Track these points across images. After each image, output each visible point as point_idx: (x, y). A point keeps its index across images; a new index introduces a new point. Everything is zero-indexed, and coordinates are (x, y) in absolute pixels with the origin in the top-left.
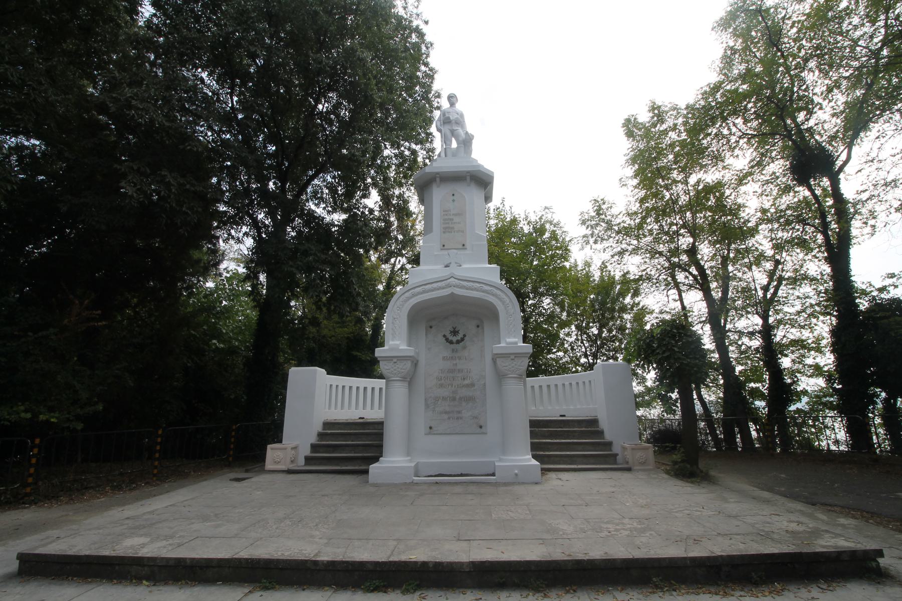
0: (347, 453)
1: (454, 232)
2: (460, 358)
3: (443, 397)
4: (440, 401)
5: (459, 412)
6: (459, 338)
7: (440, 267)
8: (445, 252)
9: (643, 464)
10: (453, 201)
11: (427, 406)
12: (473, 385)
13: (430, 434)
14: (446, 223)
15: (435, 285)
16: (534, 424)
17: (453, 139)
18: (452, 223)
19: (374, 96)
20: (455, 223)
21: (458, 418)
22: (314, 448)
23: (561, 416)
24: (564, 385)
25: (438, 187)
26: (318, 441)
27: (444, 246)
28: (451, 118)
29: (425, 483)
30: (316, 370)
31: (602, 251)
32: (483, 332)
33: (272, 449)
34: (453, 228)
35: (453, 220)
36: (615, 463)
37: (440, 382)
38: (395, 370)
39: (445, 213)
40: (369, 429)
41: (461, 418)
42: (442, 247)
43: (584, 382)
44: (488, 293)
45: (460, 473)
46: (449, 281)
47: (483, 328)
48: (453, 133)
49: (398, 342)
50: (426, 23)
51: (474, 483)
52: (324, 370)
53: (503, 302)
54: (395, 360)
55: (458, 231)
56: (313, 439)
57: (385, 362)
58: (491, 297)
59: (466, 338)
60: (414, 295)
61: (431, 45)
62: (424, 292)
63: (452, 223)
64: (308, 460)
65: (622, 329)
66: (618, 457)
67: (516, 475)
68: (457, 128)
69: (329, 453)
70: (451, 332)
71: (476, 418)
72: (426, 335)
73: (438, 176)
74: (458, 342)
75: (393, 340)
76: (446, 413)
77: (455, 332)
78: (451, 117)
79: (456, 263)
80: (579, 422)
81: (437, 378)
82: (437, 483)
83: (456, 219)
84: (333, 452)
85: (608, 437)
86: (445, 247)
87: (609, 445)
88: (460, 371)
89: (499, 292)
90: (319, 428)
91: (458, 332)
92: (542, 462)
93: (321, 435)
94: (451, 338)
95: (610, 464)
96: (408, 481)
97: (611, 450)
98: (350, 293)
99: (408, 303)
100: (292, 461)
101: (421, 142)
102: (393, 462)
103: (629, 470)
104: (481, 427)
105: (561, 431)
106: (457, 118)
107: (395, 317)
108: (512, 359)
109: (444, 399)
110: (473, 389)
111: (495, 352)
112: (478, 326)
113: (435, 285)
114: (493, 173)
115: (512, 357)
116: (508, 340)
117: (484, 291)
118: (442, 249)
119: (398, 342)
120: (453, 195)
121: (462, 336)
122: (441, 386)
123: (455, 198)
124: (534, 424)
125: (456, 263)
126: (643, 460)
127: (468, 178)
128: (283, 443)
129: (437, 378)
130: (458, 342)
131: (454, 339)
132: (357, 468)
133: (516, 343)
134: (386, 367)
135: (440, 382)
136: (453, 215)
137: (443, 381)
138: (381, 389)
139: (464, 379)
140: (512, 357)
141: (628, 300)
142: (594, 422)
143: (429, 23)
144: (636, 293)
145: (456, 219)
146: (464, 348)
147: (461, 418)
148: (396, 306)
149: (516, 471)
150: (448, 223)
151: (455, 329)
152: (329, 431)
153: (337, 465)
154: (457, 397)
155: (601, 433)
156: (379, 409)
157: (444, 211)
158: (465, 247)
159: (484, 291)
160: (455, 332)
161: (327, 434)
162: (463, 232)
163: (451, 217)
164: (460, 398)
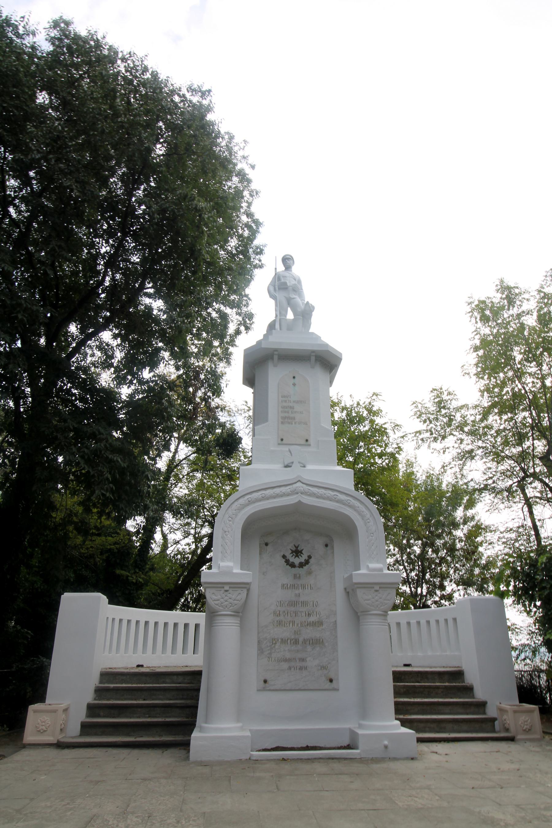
0: (139, 717)
1: (295, 423)
2: (303, 587)
3: (282, 639)
4: (278, 644)
5: (303, 660)
6: (302, 559)
7: (278, 466)
8: (286, 448)
9: (528, 731)
10: (294, 385)
11: (261, 651)
12: (320, 623)
13: (264, 689)
14: (285, 412)
15: (277, 491)
16: (398, 676)
17: (289, 309)
18: (292, 413)
19: (203, 252)
20: (296, 412)
21: (301, 668)
22: (92, 709)
23: (406, 665)
24: (409, 623)
25: (275, 366)
26: (95, 699)
27: (282, 440)
28: (288, 284)
29: (269, 760)
30: (100, 597)
31: (442, 451)
32: (333, 553)
33: (35, 711)
34: (294, 418)
35: (293, 408)
36: (494, 731)
37: (278, 618)
38: (226, 601)
39: (284, 399)
40: (164, 683)
41: (306, 668)
42: (280, 442)
43: (437, 621)
44: (344, 504)
45: (305, 746)
46: (295, 486)
47: (333, 548)
48: (290, 302)
49: (231, 564)
50: (253, 167)
51: (333, 759)
52: (105, 597)
53: (363, 517)
54: (227, 588)
55: (300, 423)
56: (89, 697)
57: (213, 590)
58: (348, 509)
59: (312, 561)
60: (250, 502)
61: (257, 193)
62: (264, 498)
63: (292, 413)
64: (86, 728)
65: (452, 549)
66: (496, 723)
67: (386, 747)
68: (294, 296)
69: (114, 717)
70: (293, 552)
71: (323, 668)
72: (260, 554)
73: (276, 353)
74: (301, 565)
75: (222, 560)
76: (286, 660)
77: (297, 552)
78: (288, 282)
79: (299, 462)
80: (441, 675)
81: (275, 613)
82: (283, 759)
83: (297, 408)
84: (118, 716)
85: (480, 694)
86: (284, 442)
87: (482, 706)
88: (304, 604)
89: (357, 504)
90: (94, 681)
91: (301, 552)
92: (418, 731)
93: (99, 692)
94: (292, 559)
95: (487, 732)
96: (244, 757)
97: (484, 713)
98: (140, 491)
99: (243, 512)
100: (61, 730)
101: (232, 305)
102: (222, 730)
103: (512, 739)
104: (331, 681)
105: (421, 687)
106: (295, 284)
107: (226, 529)
108: (376, 591)
109: (284, 641)
110: (321, 628)
111: (355, 580)
112: (326, 546)
113: (277, 491)
114: (341, 354)
115: (377, 587)
116: (372, 566)
117: (339, 501)
118: (279, 444)
119: (231, 564)
120: (294, 377)
121: (307, 558)
122: (280, 623)
123: (296, 381)
124: (398, 676)
125: (299, 462)
126: (528, 727)
127: (313, 358)
128: (48, 701)
129: (275, 613)
130: (301, 565)
131: (297, 561)
132: (157, 739)
133: (381, 570)
134: (214, 597)
135: (278, 618)
136: (294, 402)
137: (282, 618)
138: (197, 626)
139: (309, 615)
140: (377, 587)
141: (459, 513)
142: (458, 675)
143: (256, 167)
144: (471, 504)
145: (297, 408)
146: (309, 573)
147: (306, 668)
148: (227, 516)
149: (386, 742)
150: (288, 413)
151: (297, 547)
152: (112, 686)
153: (128, 735)
154: (301, 640)
155: (469, 690)
156: (153, 654)
157: (282, 397)
158: (308, 443)
159: (339, 501)
160: (297, 552)
161: (108, 690)
162: (306, 424)
163: (291, 405)
164: (305, 641)
